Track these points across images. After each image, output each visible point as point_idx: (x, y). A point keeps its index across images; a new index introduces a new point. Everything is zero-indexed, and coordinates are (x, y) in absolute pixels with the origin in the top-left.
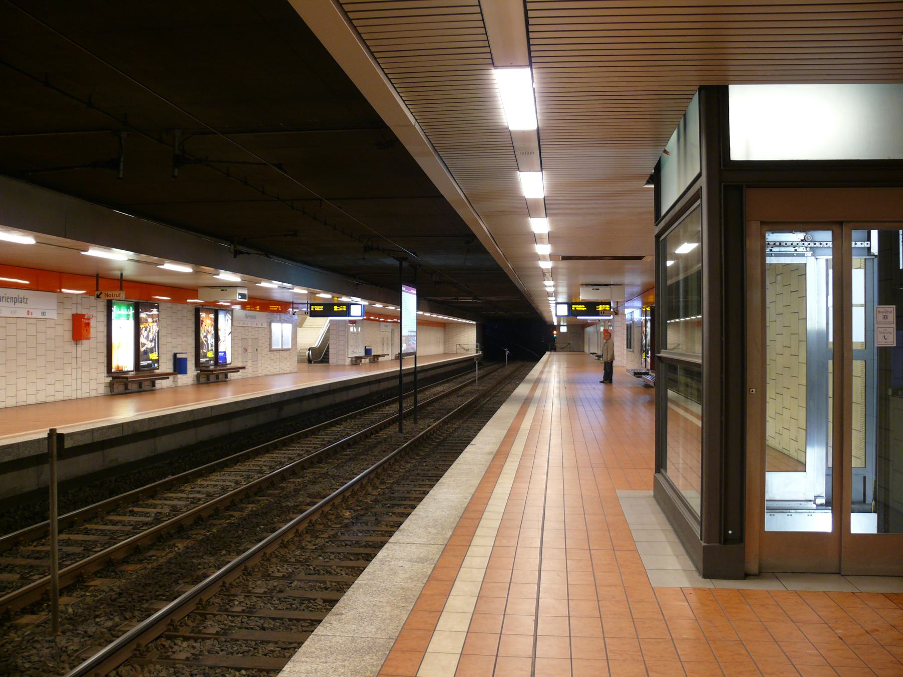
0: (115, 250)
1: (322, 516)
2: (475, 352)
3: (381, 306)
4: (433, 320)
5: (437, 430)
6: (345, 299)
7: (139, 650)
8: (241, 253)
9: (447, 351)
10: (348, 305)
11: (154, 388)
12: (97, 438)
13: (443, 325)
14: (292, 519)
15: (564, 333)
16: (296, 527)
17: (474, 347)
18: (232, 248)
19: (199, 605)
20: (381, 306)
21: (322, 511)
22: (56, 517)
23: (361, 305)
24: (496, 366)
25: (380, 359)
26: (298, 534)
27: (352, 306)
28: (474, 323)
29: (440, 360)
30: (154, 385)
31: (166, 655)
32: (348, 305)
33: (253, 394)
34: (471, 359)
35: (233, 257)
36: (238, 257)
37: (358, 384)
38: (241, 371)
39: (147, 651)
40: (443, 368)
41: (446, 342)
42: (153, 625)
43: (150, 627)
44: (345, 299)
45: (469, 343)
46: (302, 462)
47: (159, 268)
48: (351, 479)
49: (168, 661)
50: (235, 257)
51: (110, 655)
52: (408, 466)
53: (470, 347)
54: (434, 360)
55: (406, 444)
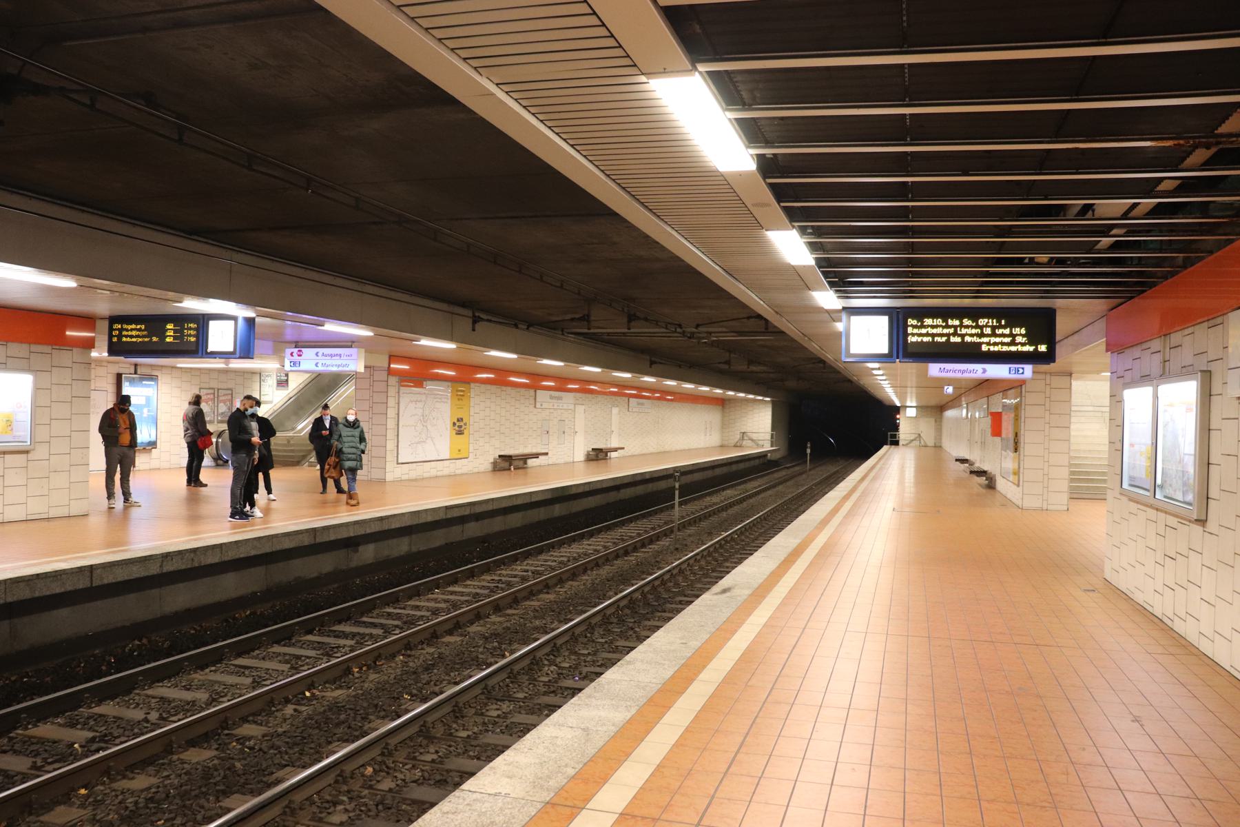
0: (211, 300)
1: (553, 650)
2: (769, 445)
3: (693, 387)
4: (715, 396)
5: (754, 525)
6: (192, 305)
7: (388, 749)
8: (655, 363)
9: (726, 443)
10: (202, 321)
11: (525, 466)
12: (618, 483)
13: (722, 402)
14: (537, 640)
15: (1047, 348)
16: (554, 641)
17: (768, 437)
18: (648, 358)
19: (423, 728)
20: (693, 387)
21: (511, 670)
22: (677, 500)
23: (234, 318)
24: (797, 468)
25: (531, 462)
26: (591, 628)
27: (212, 324)
28: (768, 399)
29: (728, 454)
30: (525, 463)
31: (370, 783)
32: (202, 321)
33: (321, 519)
34: (762, 456)
35: (648, 366)
36: (653, 366)
37: (272, 553)
38: (540, 457)
39: (352, 778)
40: (664, 481)
41: (724, 426)
42: (396, 730)
43: (284, 795)
44: (192, 305)
45: (761, 431)
46: (606, 554)
47: (486, 355)
48: (595, 606)
49: (451, 737)
50: (651, 367)
51: (471, 687)
52: (783, 515)
53: (761, 436)
54: (710, 456)
55: (692, 554)
